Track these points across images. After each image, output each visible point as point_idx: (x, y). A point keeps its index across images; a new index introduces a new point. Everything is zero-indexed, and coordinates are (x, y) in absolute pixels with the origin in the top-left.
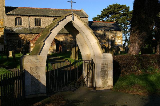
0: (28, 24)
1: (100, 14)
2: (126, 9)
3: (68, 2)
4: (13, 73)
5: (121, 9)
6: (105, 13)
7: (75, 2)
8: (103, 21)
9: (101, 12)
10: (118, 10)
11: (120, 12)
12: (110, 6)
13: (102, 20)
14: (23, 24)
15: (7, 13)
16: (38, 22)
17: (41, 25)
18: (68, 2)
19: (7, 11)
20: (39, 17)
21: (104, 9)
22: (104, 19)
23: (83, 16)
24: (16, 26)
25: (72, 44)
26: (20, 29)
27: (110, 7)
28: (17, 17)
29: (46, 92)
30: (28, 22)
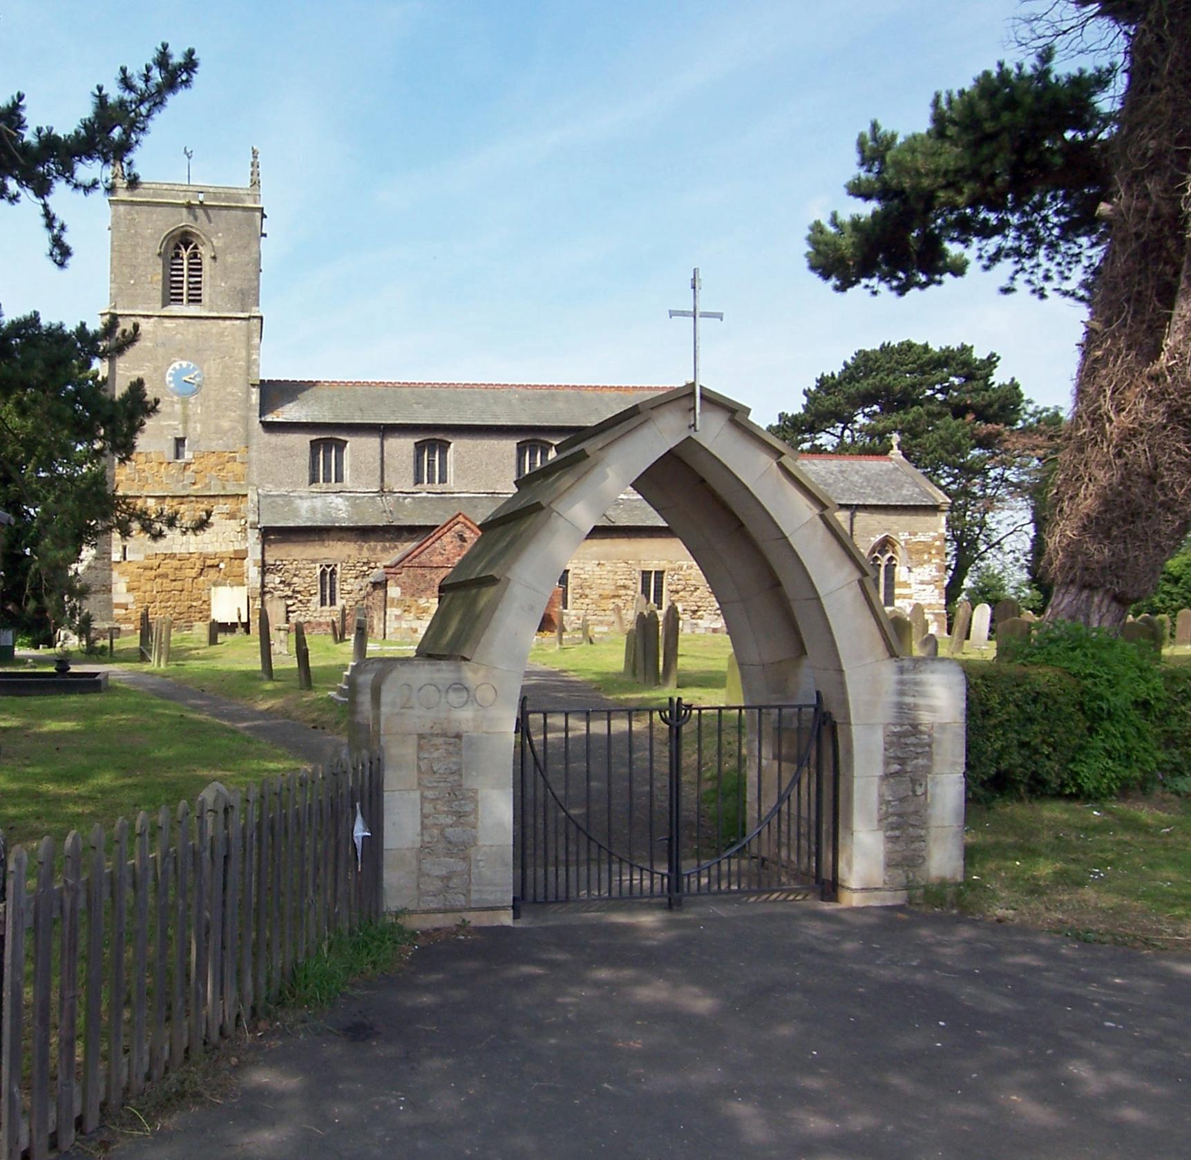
0: (379, 473)
1: (796, 406)
2: (969, 378)
3: (672, 314)
4: (923, 746)
5: (939, 375)
6: (828, 402)
7: (720, 316)
8: (817, 450)
9: (804, 400)
10: (919, 377)
11: (929, 392)
12: (863, 356)
13: (806, 446)
14: (347, 472)
15: (269, 418)
16: (434, 466)
17: (445, 482)
18: (672, 314)
19: (266, 405)
20: (438, 436)
21: (822, 382)
22: (826, 440)
23: (735, 414)
24: (314, 488)
25: (625, 587)
26: (338, 501)
27: (864, 363)
28: (314, 437)
29: (509, 899)
30: (379, 462)
